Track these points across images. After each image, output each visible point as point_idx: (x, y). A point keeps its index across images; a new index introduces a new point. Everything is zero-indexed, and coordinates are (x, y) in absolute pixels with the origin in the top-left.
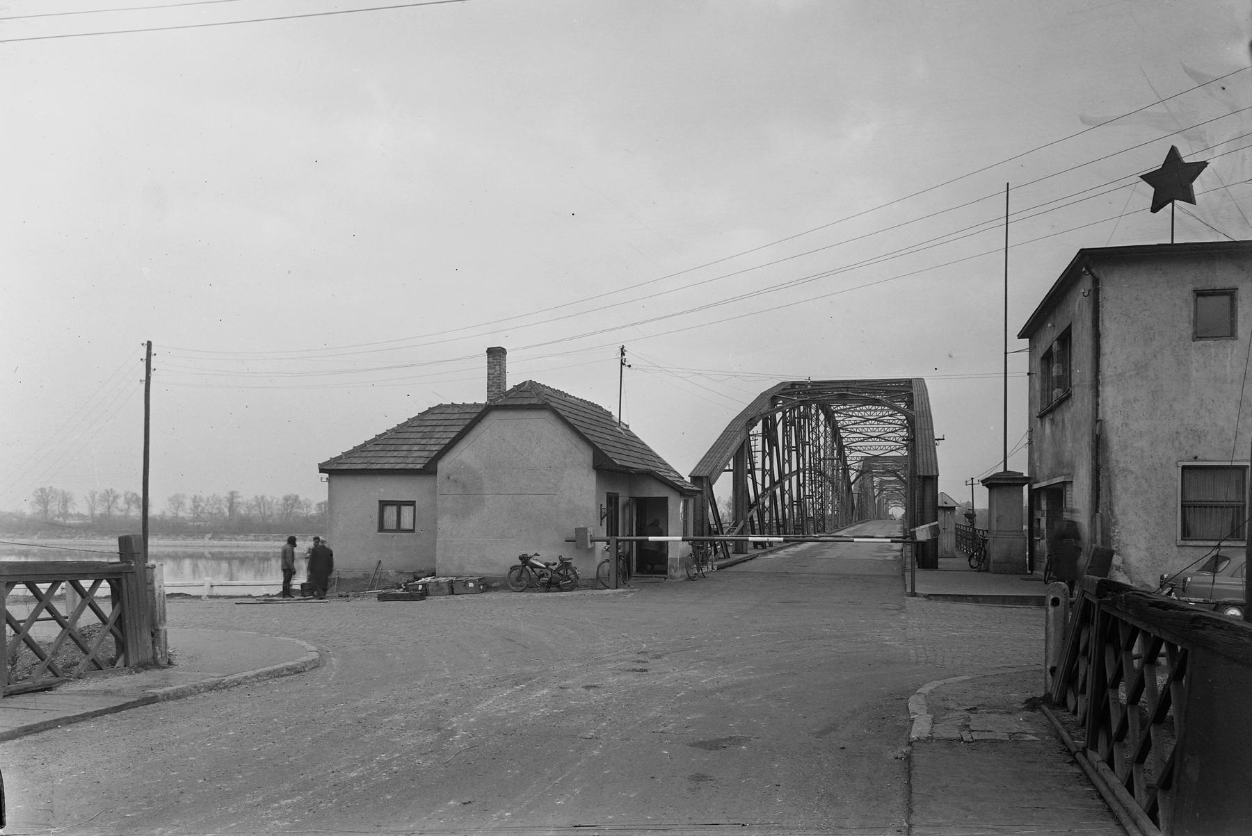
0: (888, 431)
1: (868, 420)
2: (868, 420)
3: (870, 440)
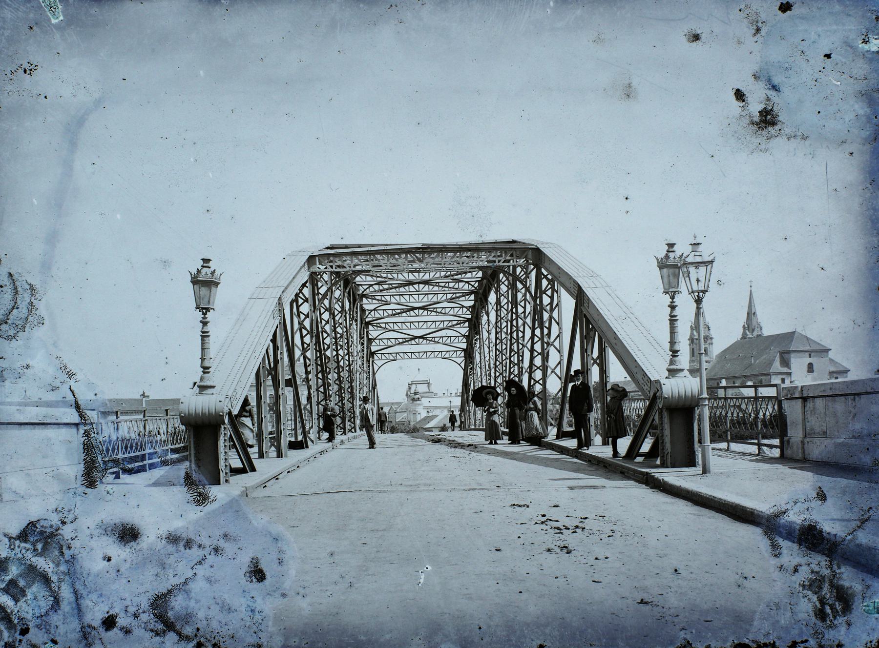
0: (441, 326)
1: (414, 309)
2: (414, 309)
3: (413, 342)
